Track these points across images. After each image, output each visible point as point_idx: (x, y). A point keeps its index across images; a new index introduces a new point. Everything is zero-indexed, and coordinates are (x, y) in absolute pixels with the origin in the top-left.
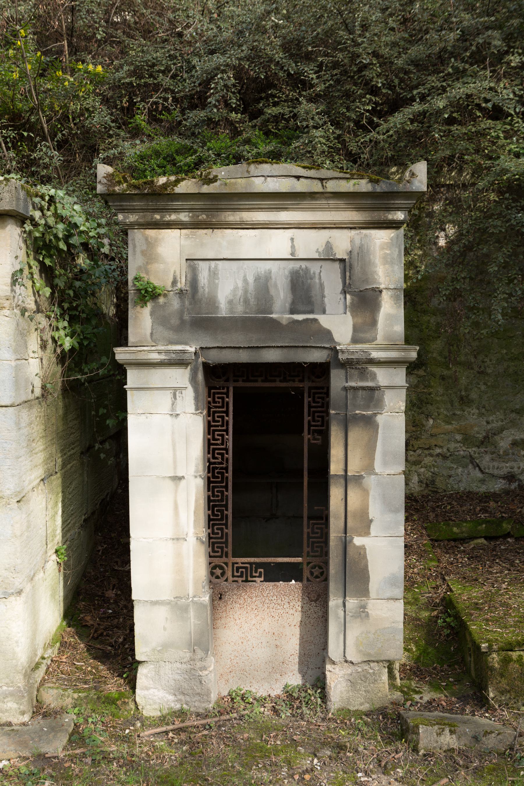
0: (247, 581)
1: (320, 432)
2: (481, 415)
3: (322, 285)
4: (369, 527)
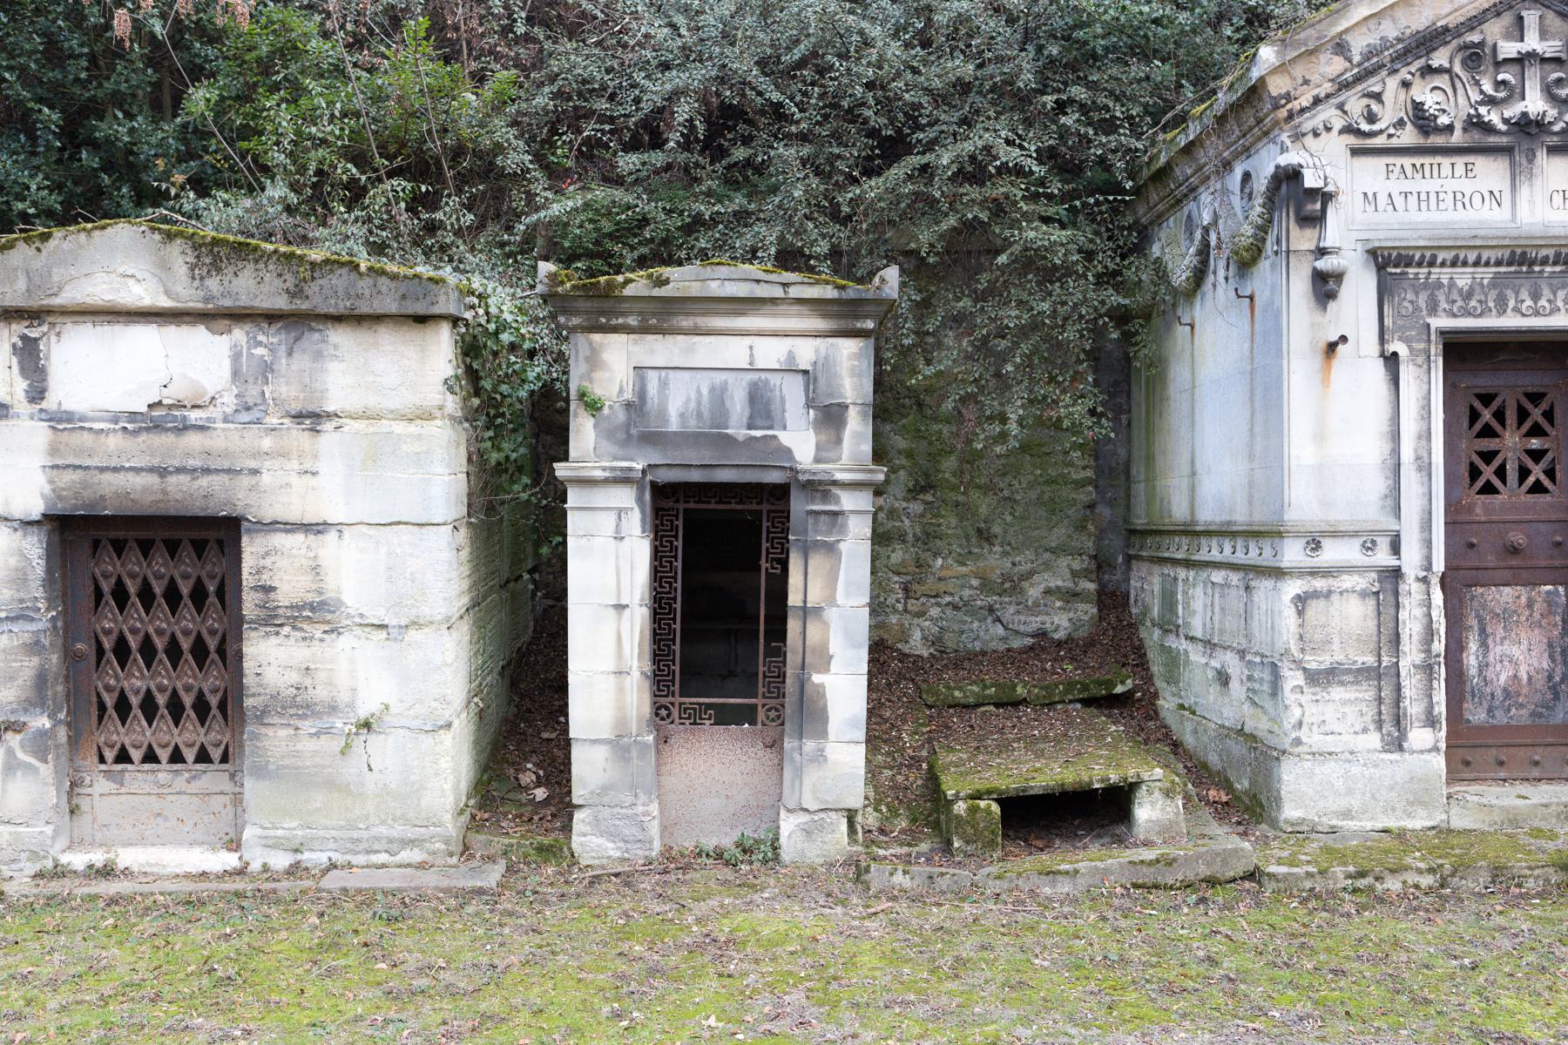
0: (695, 723)
1: (779, 561)
2: (1005, 554)
3: (783, 399)
4: (829, 663)
